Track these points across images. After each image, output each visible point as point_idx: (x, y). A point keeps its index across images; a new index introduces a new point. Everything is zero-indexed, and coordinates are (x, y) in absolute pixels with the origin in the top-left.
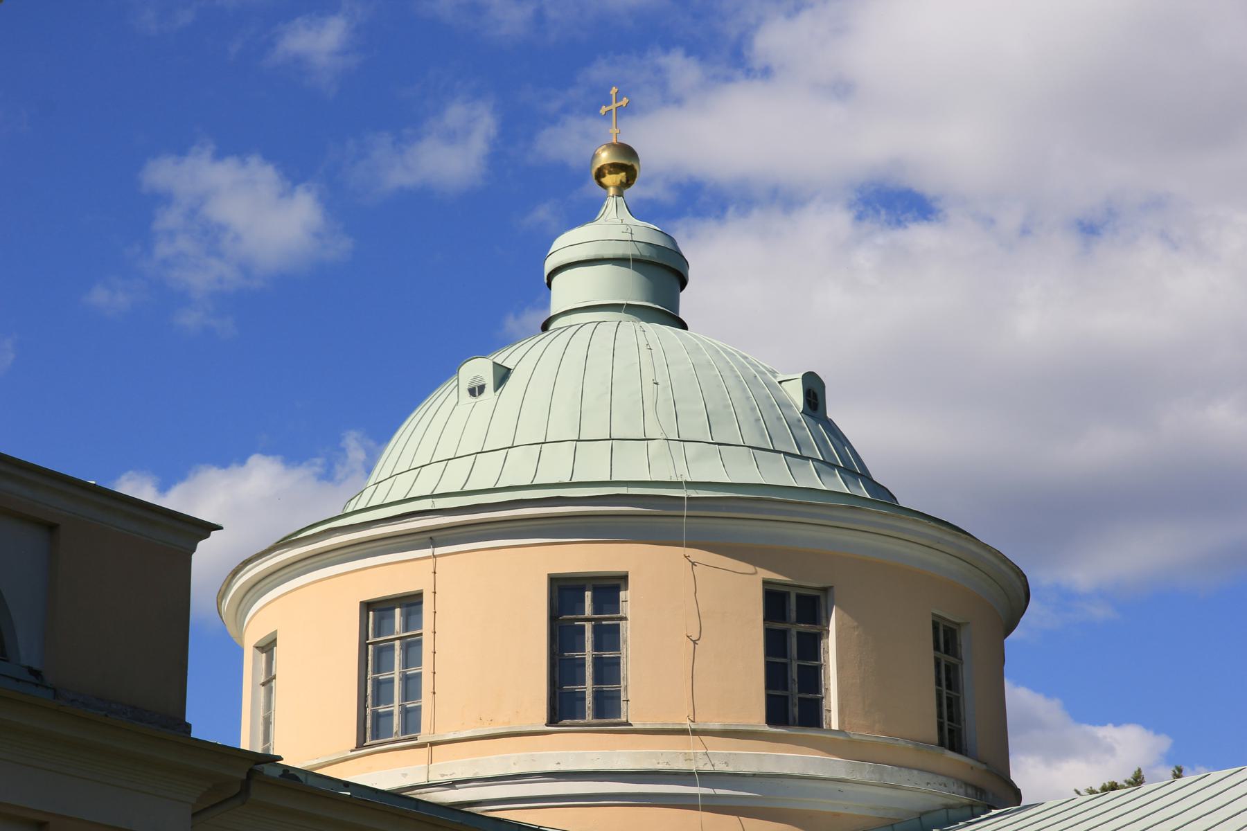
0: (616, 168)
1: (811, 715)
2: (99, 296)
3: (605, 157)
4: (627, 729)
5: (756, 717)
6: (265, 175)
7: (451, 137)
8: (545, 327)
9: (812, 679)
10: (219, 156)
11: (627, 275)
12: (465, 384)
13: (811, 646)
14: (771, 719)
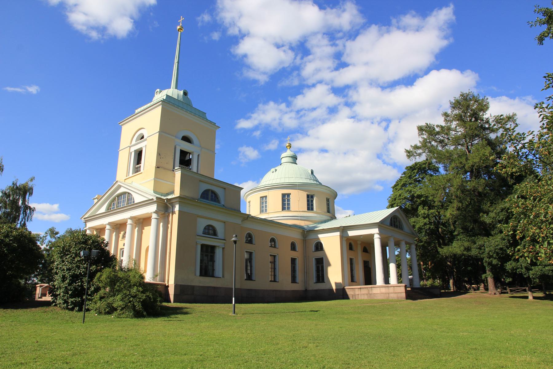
0: (289, 146)
4: (291, 211)
5: (306, 210)
9: (312, 205)
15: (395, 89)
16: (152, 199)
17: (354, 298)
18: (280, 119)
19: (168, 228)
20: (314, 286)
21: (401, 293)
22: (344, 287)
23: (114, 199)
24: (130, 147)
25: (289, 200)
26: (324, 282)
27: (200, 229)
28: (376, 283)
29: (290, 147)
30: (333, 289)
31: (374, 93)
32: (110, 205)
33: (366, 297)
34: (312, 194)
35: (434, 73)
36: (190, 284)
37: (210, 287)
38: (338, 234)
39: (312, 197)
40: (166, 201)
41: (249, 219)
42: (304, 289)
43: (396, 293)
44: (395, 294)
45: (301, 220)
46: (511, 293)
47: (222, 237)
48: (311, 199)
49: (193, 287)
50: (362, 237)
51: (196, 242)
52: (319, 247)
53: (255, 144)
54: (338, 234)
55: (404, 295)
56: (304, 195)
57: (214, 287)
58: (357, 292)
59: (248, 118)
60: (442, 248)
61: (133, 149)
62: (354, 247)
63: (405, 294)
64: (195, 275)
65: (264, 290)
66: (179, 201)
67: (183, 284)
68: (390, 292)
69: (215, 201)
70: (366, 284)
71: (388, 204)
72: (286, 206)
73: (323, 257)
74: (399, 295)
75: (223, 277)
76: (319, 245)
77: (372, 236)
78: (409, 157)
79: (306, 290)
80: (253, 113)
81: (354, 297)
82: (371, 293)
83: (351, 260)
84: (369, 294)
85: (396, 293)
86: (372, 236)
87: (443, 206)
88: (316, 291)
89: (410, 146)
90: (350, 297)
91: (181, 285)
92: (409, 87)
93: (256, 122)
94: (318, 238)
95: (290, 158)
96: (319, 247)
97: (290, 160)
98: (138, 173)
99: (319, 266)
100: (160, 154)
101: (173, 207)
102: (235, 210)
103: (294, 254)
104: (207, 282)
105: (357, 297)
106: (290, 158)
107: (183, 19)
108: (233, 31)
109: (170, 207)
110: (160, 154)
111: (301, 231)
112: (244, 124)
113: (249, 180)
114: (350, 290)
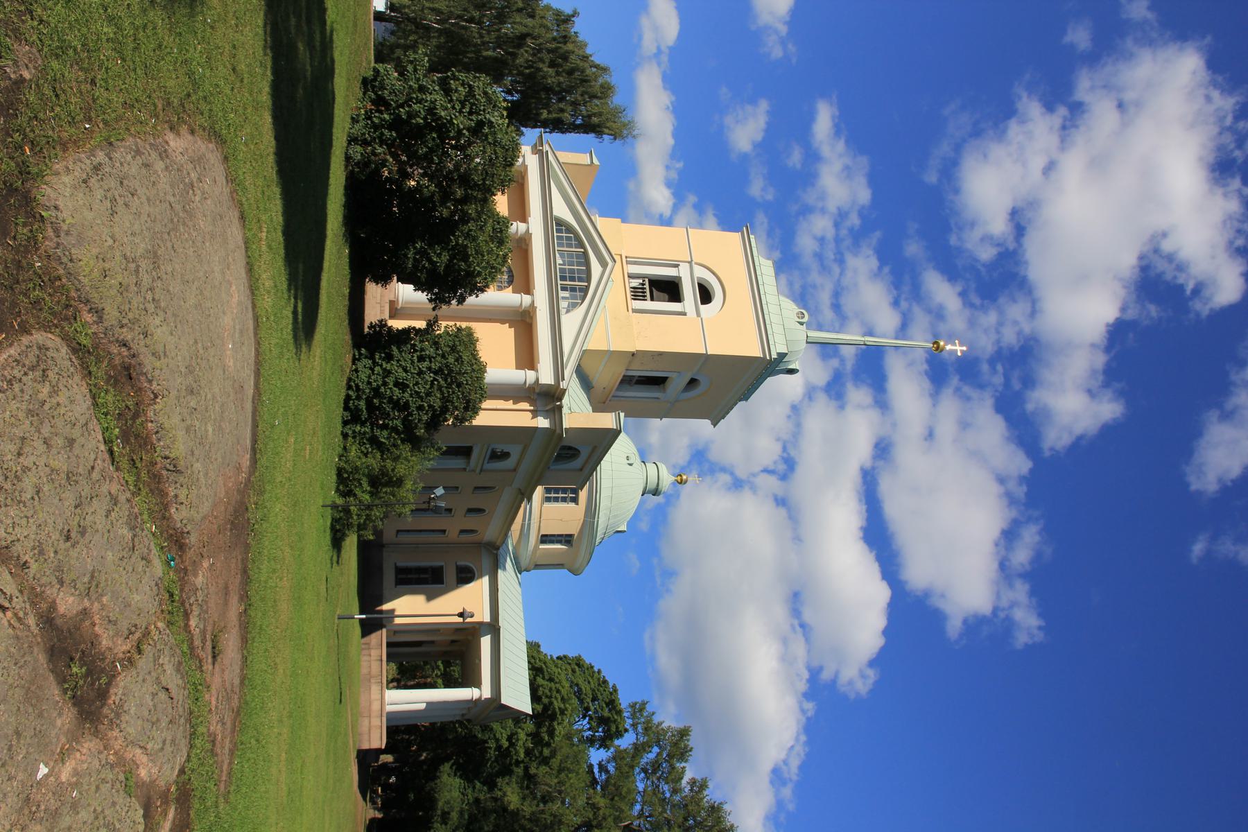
0: (682, 480)
1: (543, 542)
2: (724, 90)
3: (684, 477)
4: (542, 504)
5: (543, 532)
6: (759, 137)
7: (763, 189)
8: (644, 462)
9: (552, 542)
10: (767, 123)
11: (654, 486)
12: (632, 456)
13: (559, 542)
14: (543, 536)
15: (860, 501)
16: (563, 379)
17: (363, 646)
18: (823, 211)
19: (506, 398)
20: (390, 562)
21: (370, 741)
22: (385, 626)
23: (581, 245)
24: (690, 263)
25: (564, 500)
29: (680, 483)
30: (381, 604)
31: (860, 450)
32: (569, 229)
33: (364, 671)
35: (880, 593)
38: (487, 619)
40: (558, 403)
41: (520, 496)
43: (370, 730)
44: (367, 729)
45: (523, 525)
47: (485, 467)
50: (477, 661)
52: (463, 575)
53: (769, 147)
54: (487, 619)
55: (365, 746)
56: (573, 528)
58: (375, 653)
59: (837, 131)
60: (451, 768)
61: (683, 273)
66: (555, 431)
68: (372, 720)
70: (388, 728)
71: (551, 649)
72: (553, 495)
73: (444, 586)
74: (366, 737)
76: (469, 575)
77: (477, 684)
78: (633, 706)
80: (847, 142)
81: (366, 646)
82: (373, 681)
84: (369, 677)
85: (370, 730)
86: (477, 684)
87: (529, 780)
88: (380, 569)
89: (654, 710)
90: (366, 639)
92: (861, 534)
93: (826, 151)
94: (481, 576)
96: (465, 576)
97: (652, 484)
98: (629, 295)
101: (547, 411)
105: (366, 652)
107: (957, 341)
108: (1084, 86)
109: (547, 405)
111: (498, 544)
112: (824, 120)
113: (676, 142)
114: (380, 639)
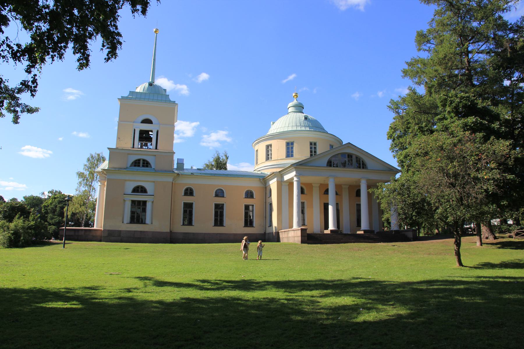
20: (181, 228)
26: (223, 226)
27: (129, 190)
28: (293, 226)
34: (292, 141)
36: (117, 229)
37: (137, 231)
39: (292, 143)
42: (263, 232)
43: (297, 237)
46: (516, 237)
48: (312, 146)
49: (120, 232)
51: (124, 200)
57: (141, 231)
62: (305, 191)
63: (300, 237)
64: (123, 222)
65: (205, 234)
67: (111, 229)
69: (147, 166)
75: (152, 223)
79: (265, 233)
83: (303, 203)
91: (108, 230)
95: (293, 108)
99: (218, 211)
100: (119, 138)
102: (170, 171)
103: (249, 201)
104: (219, 230)
106: (293, 108)
110: (119, 138)
